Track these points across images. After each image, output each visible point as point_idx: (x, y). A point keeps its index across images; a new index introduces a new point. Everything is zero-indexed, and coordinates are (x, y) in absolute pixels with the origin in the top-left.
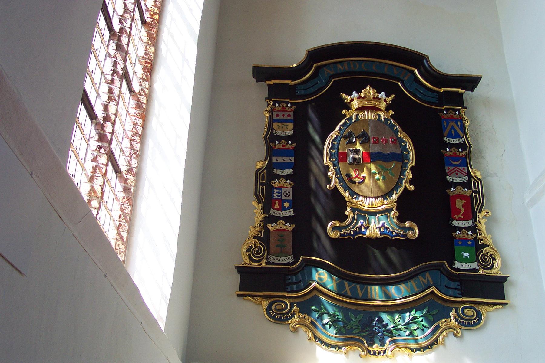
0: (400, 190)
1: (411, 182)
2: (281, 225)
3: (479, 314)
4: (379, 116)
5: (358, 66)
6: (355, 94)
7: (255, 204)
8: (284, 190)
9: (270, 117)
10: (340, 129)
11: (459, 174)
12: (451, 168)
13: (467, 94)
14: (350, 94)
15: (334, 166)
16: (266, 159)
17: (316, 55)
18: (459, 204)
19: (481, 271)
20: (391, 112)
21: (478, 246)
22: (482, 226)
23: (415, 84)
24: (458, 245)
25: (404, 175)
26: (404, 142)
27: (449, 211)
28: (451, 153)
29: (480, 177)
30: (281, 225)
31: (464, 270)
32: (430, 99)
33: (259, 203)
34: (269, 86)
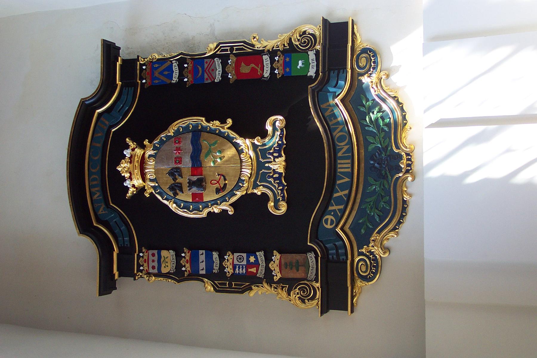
0: (232, 134)
1: (223, 122)
3: (365, 51)
4: (150, 156)
6: (127, 183)
7: (252, 294)
8: (236, 262)
11: (212, 67)
12: (206, 76)
13: (124, 54)
14: (127, 188)
17: (84, 224)
18: (245, 69)
19: (318, 47)
20: (146, 142)
21: (290, 50)
22: (270, 44)
24: (290, 72)
25: (216, 130)
27: (254, 82)
28: (190, 76)
29: (215, 45)
32: (130, 98)
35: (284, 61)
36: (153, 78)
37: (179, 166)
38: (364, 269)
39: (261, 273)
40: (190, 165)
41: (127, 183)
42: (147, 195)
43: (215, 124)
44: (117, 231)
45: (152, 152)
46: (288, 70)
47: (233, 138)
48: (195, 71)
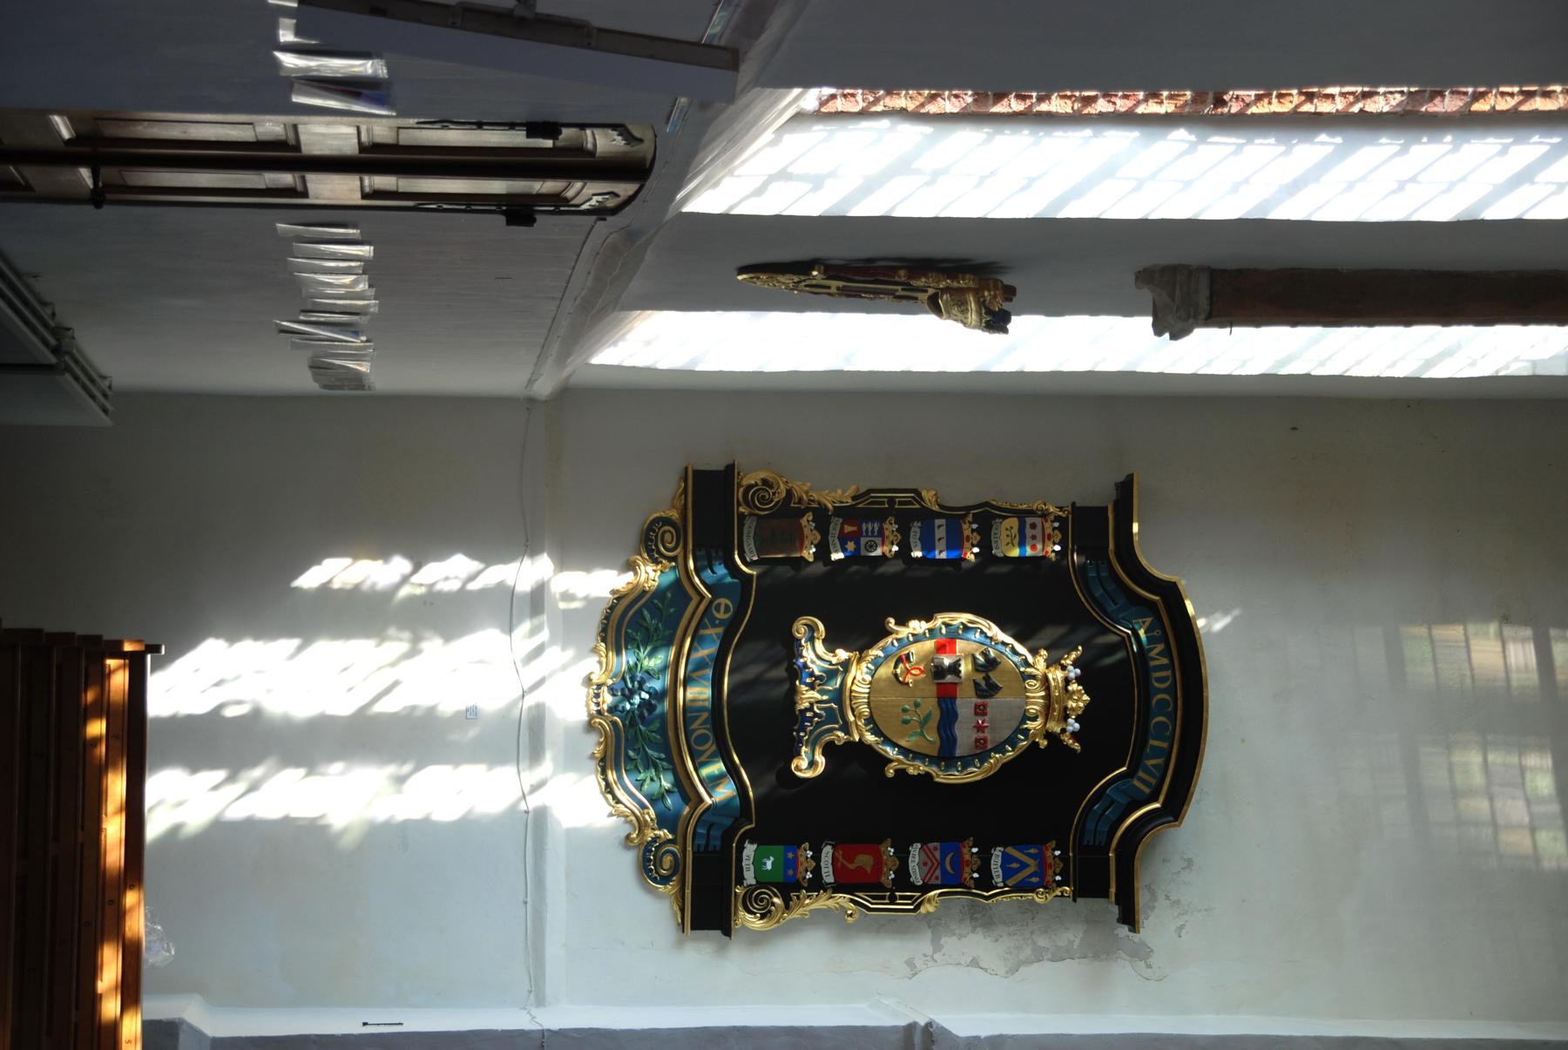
1: (901, 773)
2: (811, 538)
3: (664, 880)
4: (1034, 719)
5: (1162, 686)
6: (1074, 672)
7: (851, 491)
8: (878, 540)
9: (1031, 513)
10: (1004, 644)
11: (926, 869)
12: (938, 854)
14: (1075, 664)
15: (931, 630)
16: (941, 506)
18: (864, 861)
20: (1044, 743)
21: (789, 888)
22: (823, 902)
23: (1123, 800)
24: (786, 852)
25: (914, 759)
26: (982, 763)
27: (847, 840)
28: (967, 857)
29: (922, 910)
30: (811, 538)
31: (739, 860)
32: (1090, 826)
33: (854, 498)
34: (1106, 509)
35: (796, 870)
36: (1040, 858)
37: (980, 701)
38: (668, 537)
39: (836, 523)
40: (958, 701)
41: (1074, 672)
42: (1044, 652)
43: (916, 768)
44: (1111, 587)
45: (1030, 725)
46: (790, 855)
47: (883, 743)
48: (959, 863)
